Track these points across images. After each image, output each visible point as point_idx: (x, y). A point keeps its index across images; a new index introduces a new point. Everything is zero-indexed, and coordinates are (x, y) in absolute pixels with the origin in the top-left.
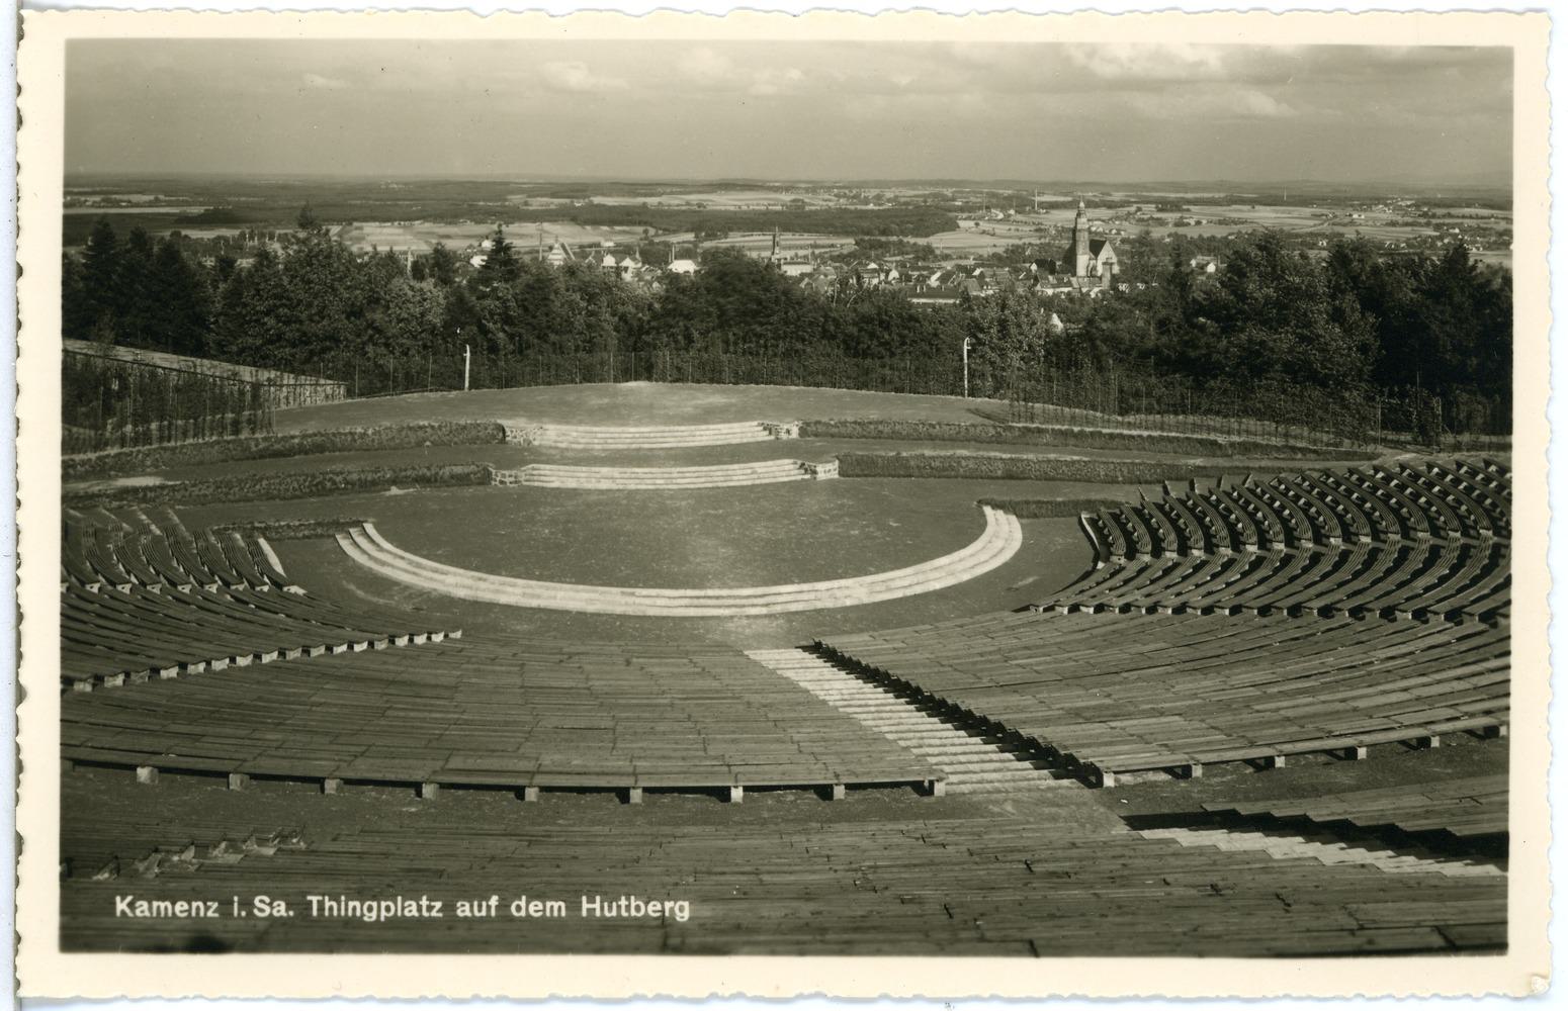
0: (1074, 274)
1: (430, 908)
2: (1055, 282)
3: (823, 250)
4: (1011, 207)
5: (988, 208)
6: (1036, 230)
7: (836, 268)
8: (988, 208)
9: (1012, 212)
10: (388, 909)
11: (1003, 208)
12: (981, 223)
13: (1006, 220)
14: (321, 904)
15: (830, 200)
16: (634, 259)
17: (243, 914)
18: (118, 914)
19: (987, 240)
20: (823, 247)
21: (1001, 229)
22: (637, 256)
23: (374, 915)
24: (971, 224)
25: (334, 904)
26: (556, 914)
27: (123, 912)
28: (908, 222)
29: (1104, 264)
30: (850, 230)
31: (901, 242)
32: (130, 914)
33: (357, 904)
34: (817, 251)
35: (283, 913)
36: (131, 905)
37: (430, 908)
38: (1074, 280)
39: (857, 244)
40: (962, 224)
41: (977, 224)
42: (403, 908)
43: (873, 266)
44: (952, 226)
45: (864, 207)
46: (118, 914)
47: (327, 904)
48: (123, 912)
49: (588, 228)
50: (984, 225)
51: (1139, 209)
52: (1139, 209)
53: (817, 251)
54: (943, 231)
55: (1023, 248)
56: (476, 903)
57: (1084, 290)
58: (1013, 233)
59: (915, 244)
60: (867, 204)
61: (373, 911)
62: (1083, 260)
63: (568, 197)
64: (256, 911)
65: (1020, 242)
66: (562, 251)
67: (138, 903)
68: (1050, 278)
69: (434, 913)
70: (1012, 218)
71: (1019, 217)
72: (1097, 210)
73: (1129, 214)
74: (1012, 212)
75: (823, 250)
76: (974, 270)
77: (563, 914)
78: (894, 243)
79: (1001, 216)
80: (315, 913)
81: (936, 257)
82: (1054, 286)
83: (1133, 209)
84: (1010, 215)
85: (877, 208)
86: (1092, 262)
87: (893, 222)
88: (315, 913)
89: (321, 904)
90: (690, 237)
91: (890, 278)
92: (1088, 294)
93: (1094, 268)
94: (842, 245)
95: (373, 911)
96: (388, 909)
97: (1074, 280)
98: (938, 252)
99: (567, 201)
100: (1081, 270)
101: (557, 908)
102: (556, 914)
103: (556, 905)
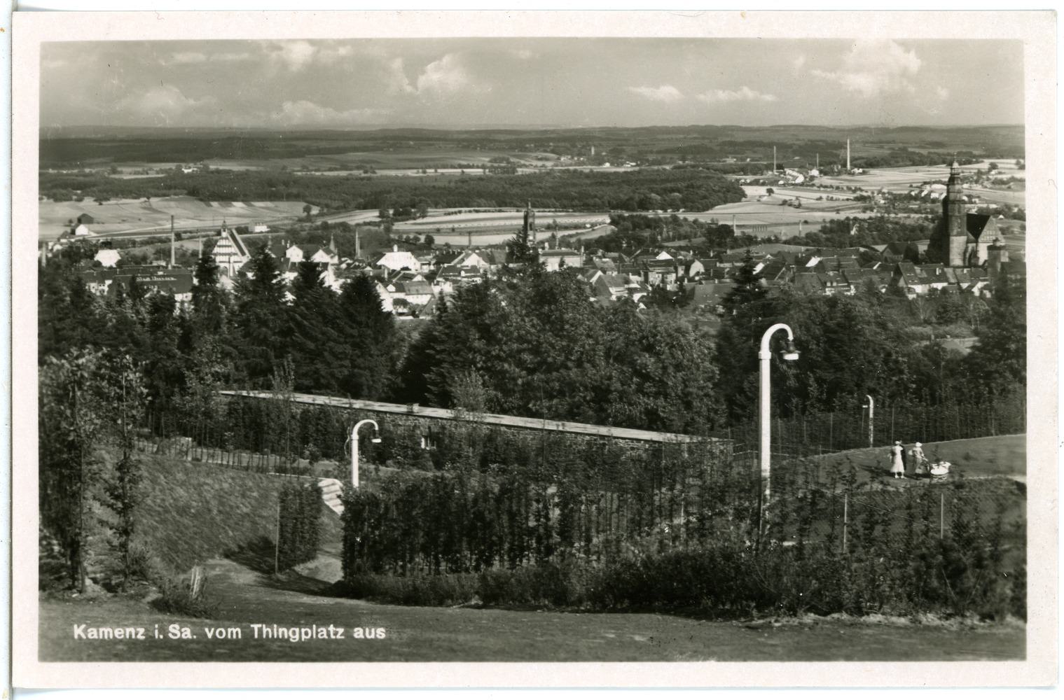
0: (947, 264)
1: (336, 634)
2: (924, 275)
3: (567, 233)
4: (813, 165)
5: (780, 167)
6: (857, 199)
7: (614, 260)
8: (780, 167)
9: (815, 172)
10: (306, 634)
11: (802, 168)
12: (774, 188)
13: (808, 184)
14: (260, 630)
15: (547, 159)
16: (328, 252)
17: (161, 637)
18: (76, 637)
19: (791, 214)
20: (566, 228)
21: (808, 197)
22: (332, 247)
23: (297, 637)
24: (762, 190)
25: (269, 630)
26: (234, 637)
27: (79, 635)
28: (673, 190)
29: (990, 248)
30: (591, 201)
31: (675, 219)
32: (84, 637)
33: (285, 630)
34: (560, 234)
35: (189, 636)
36: (85, 631)
37: (336, 634)
38: (949, 271)
39: (613, 222)
40: (750, 191)
41: (770, 191)
42: (317, 633)
43: (664, 256)
44: (736, 194)
45: (596, 169)
46: (76, 637)
47: (265, 630)
48: (79, 635)
49: (215, 204)
50: (781, 194)
51: (993, 166)
52: (993, 166)
53: (560, 234)
54: (725, 202)
55: (844, 226)
56: (367, 630)
57: (965, 286)
58: (825, 203)
59: (695, 221)
60: (601, 163)
61: (295, 635)
62: (958, 243)
63: (172, 161)
64: (170, 635)
65: (842, 216)
66: (231, 243)
67: (89, 630)
68: (918, 269)
69: (338, 637)
70: (816, 182)
71: (827, 180)
72: (933, 168)
73: (980, 173)
74: (815, 172)
75: (567, 233)
76: (808, 260)
77: (240, 637)
78: (666, 221)
79: (800, 179)
80: (256, 636)
81: (735, 239)
82: (922, 281)
83: (985, 165)
84: (812, 178)
85: (614, 170)
86: (971, 246)
87: (652, 190)
88: (256, 636)
89: (260, 630)
90: (372, 215)
91: (692, 273)
92: (969, 291)
93: (974, 254)
94: (593, 225)
95: (295, 635)
96: (306, 634)
97: (949, 271)
98: (737, 233)
99: (172, 166)
100: (956, 260)
101: (235, 632)
102: (234, 637)
103: (235, 631)
